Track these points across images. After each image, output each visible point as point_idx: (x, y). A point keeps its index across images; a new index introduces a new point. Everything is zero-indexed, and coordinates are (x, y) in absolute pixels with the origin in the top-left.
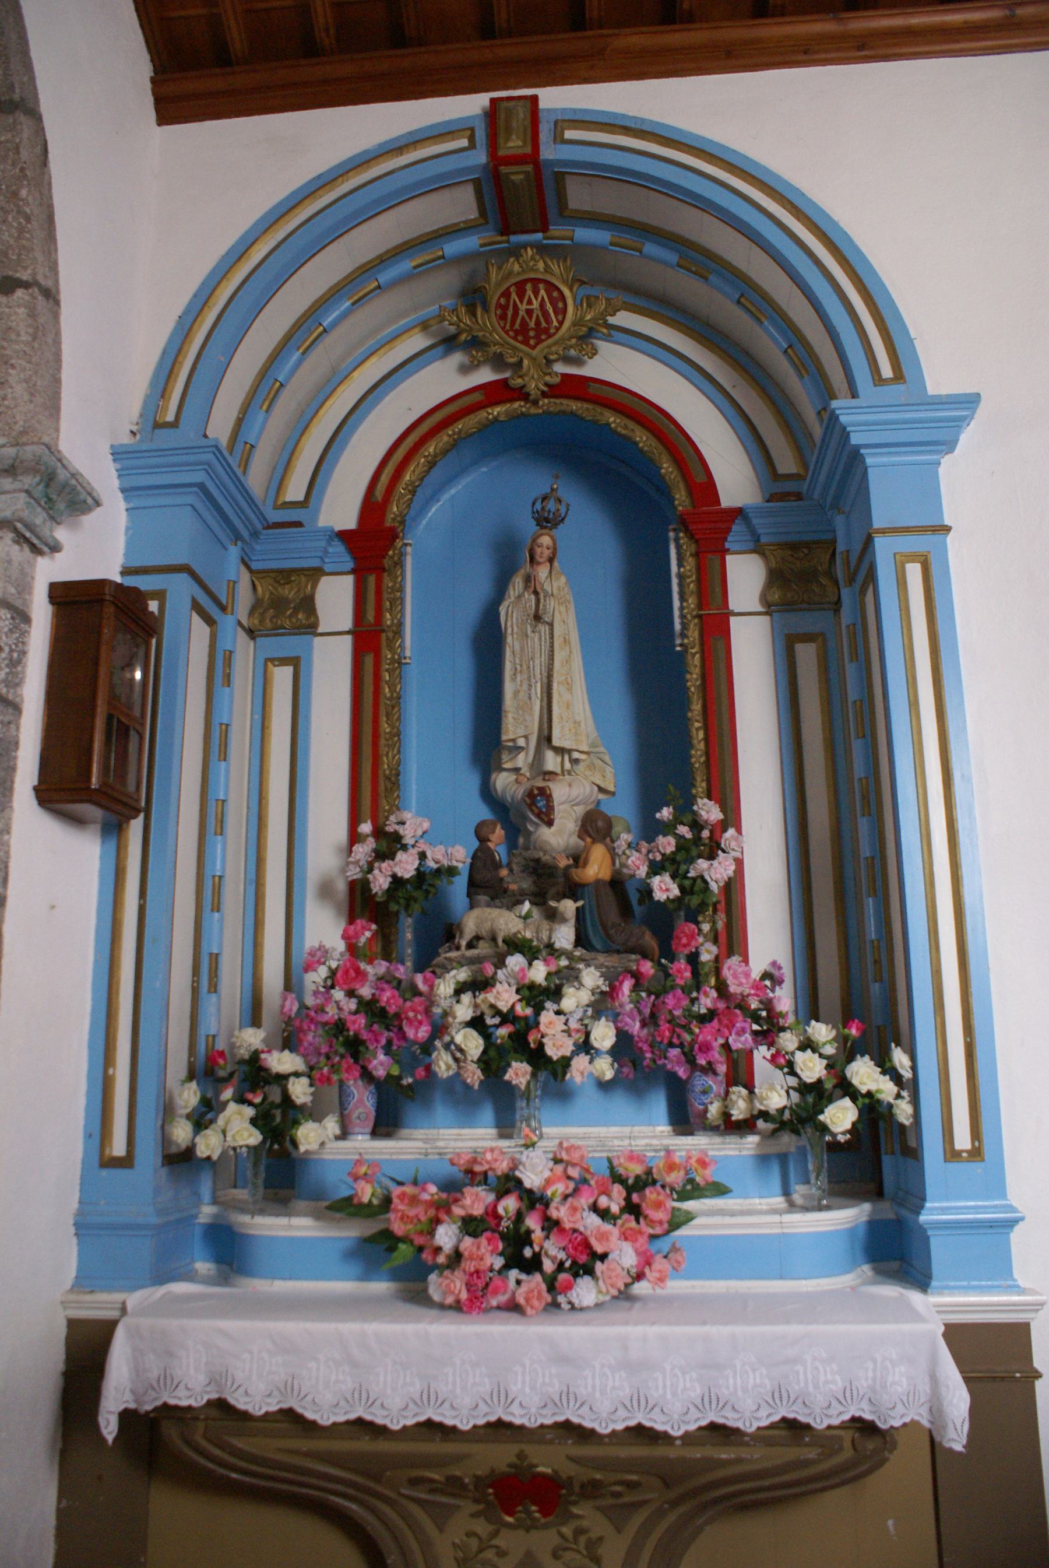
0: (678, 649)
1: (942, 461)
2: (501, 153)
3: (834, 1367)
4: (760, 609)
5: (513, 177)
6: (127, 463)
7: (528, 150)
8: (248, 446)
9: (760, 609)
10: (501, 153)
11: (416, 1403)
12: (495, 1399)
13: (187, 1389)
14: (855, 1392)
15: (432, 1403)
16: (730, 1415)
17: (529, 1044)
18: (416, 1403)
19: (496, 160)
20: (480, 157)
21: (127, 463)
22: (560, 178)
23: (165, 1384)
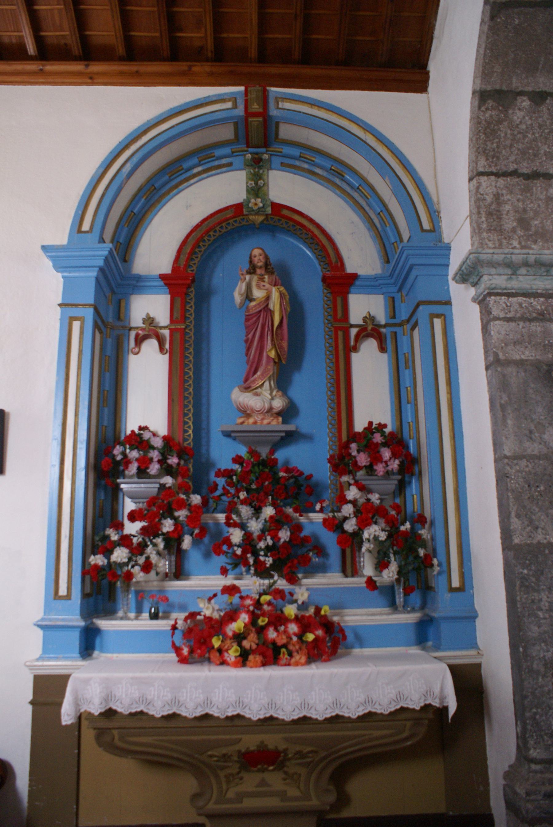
0: (282, 474)
1: (385, 356)
2: (250, 110)
3: (297, 693)
4: (400, 293)
5: (257, 107)
6: (106, 269)
7: (261, 110)
8: (153, 188)
9: (400, 293)
10: (250, 110)
11: (169, 704)
12: (335, 705)
13: (380, 705)
14: (402, 696)
15: (306, 708)
16: (377, 706)
17: (274, 571)
18: (169, 704)
19: (248, 114)
20: (240, 111)
21: (106, 269)
22: (277, 124)
23: (400, 699)
